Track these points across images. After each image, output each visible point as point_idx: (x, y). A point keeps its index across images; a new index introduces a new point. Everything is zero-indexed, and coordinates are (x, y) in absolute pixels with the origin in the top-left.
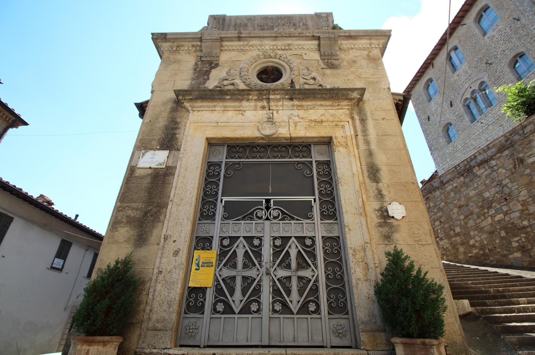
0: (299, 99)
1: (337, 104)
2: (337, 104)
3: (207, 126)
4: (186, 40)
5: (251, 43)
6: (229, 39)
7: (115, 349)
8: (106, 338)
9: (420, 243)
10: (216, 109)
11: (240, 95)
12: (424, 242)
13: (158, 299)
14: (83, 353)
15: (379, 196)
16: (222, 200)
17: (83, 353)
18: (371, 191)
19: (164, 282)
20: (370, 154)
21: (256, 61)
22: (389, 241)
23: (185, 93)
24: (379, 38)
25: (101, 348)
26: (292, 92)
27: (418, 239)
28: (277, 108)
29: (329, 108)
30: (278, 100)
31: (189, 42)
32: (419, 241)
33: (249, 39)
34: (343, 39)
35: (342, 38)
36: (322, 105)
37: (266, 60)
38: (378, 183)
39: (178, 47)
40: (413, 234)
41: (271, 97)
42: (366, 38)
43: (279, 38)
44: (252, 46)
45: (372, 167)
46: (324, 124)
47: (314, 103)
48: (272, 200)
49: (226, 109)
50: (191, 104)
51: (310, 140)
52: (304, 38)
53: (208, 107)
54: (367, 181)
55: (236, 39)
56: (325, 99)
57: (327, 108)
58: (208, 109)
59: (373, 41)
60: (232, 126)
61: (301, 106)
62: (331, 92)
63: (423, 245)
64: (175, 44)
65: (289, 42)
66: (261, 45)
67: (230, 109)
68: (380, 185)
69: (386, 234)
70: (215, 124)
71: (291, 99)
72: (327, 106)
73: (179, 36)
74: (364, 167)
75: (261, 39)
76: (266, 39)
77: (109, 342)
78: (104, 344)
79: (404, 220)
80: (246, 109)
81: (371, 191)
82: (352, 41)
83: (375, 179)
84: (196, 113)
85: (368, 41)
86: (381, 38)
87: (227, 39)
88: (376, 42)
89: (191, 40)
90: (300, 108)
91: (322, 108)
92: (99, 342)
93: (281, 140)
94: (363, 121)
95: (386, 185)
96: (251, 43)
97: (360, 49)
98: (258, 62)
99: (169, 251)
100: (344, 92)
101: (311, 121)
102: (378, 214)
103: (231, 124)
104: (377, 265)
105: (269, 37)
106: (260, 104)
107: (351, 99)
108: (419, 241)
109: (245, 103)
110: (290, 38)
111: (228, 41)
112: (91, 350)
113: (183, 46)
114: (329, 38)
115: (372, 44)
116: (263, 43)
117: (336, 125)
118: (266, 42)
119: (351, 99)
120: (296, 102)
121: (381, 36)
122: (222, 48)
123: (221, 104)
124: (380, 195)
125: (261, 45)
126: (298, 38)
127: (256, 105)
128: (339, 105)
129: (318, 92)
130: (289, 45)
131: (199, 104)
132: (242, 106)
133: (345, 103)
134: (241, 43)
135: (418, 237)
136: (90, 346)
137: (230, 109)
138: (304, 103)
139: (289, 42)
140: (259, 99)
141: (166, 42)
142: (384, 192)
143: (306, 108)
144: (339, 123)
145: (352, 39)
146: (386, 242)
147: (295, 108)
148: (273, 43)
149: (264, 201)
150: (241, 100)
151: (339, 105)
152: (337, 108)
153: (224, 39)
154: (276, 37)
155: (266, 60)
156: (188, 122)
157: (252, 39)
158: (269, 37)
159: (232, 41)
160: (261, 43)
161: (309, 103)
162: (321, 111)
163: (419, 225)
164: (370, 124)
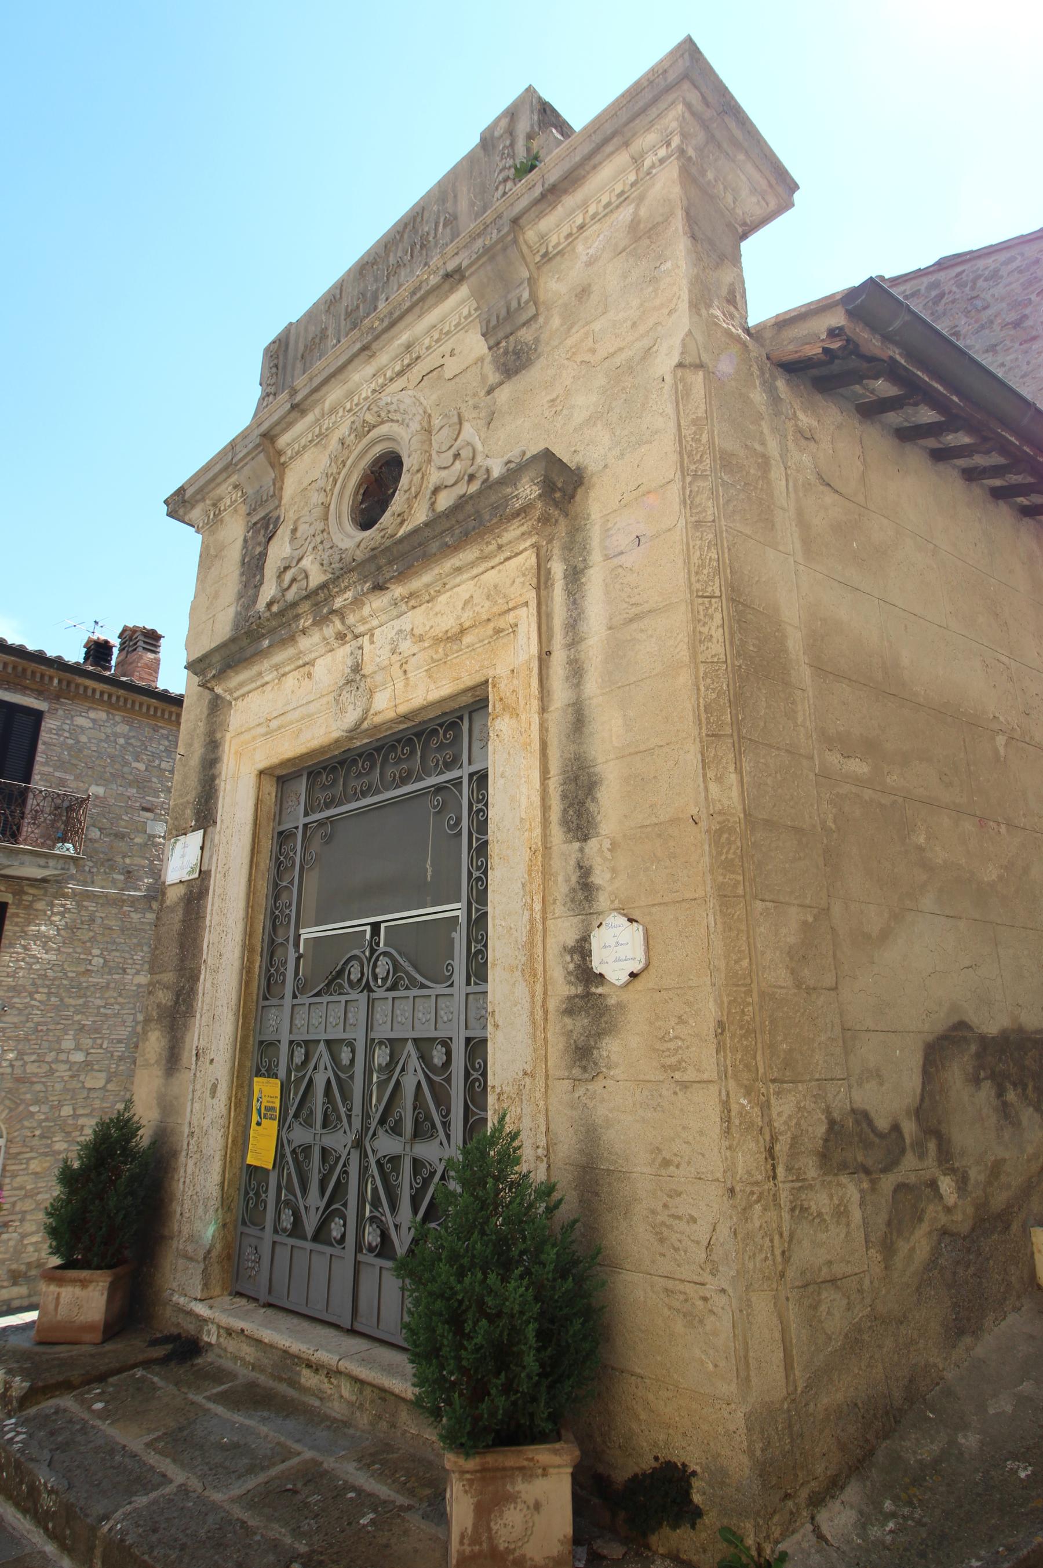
0: (401, 577)
1: (493, 547)
2: (493, 547)
3: (254, 738)
4: (218, 480)
5: (327, 405)
6: (283, 425)
7: (102, 1294)
8: (85, 1274)
9: (677, 1076)
10: (267, 679)
11: (282, 625)
12: (691, 1075)
13: (190, 1193)
14: (50, 1298)
15: (580, 895)
16: (298, 937)
17: (50, 1298)
18: (560, 879)
19: (198, 1156)
20: (579, 721)
21: (344, 463)
22: (585, 1069)
23: (202, 665)
24: (653, 112)
25: (77, 1291)
26: (373, 568)
27: (673, 1060)
28: (367, 626)
29: (481, 569)
30: (357, 602)
31: (225, 480)
32: (675, 1068)
33: (316, 396)
34: (540, 216)
35: (532, 214)
36: (458, 570)
37: (365, 441)
38: (585, 839)
39: (214, 505)
40: (662, 1039)
41: (338, 603)
42: (609, 148)
43: (374, 346)
44: (333, 410)
45: (576, 778)
46: (467, 639)
47: (437, 570)
48: (383, 925)
49: (281, 671)
50: (224, 685)
51: (454, 705)
52: (431, 300)
53: (252, 680)
54: (557, 833)
55: (294, 415)
56: (455, 548)
57: (475, 571)
58: (253, 685)
59: (636, 146)
60: (291, 723)
61: (411, 594)
62: (461, 517)
63: (685, 1085)
64: (208, 502)
65: (404, 338)
66: (349, 395)
67: (287, 669)
68: (593, 844)
69: (580, 1044)
70: (263, 730)
71: (379, 588)
72: (473, 564)
73: (202, 481)
74: (554, 784)
75: (340, 377)
76: (350, 367)
77: (91, 1282)
78: (84, 1284)
79: (639, 984)
80: (313, 656)
81: (560, 879)
82: (569, 201)
83: (579, 827)
84: (240, 703)
85: (622, 158)
86: (662, 105)
87: (278, 428)
88: (651, 138)
89: (225, 475)
90: (412, 603)
91: (465, 576)
92: (73, 1281)
93: (391, 728)
94: (575, 576)
95: (607, 844)
96: (327, 405)
97: (610, 209)
98: (349, 463)
99: (203, 1086)
100: (493, 498)
101: (437, 641)
102: (571, 966)
103: (290, 717)
104: (540, 1152)
105: (350, 361)
106: (329, 631)
107: (524, 511)
108: (675, 1068)
109: (304, 643)
110: (401, 325)
111: (285, 430)
112: (63, 1295)
113: (221, 499)
114: (487, 250)
115: (642, 155)
116: (350, 385)
117: (498, 631)
118: (356, 377)
119: (524, 511)
120: (398, 591)
121: (655, 100)
122: (282, 460)
123: (266, 664)
124: (585, 888)
125: (349, 395)
126: (417, 310)
127: (325, 639)
128: (500, 547)
129: (427, 533)
130: (408, 347)
131: (235, 679)
132: (301, 652)
133: (513, 532)
134: (310, 418)
135: (677, 1050)
136: (61, 1286)
137: (287, 669)
138: (416, 584)
139: (404, 338)
140: (321, 621)
141: (193, 507)
142: (600, 877)
143: (427, 598)
144: (501, 623)
145: (565, 191)
146: (576, 1072)
147: (404, 608)
148: (369, 370)
149: (368, 928)
150: (292, 639)
151: (500, 547)
152: (501, 557)
153: (273, 433)
154: (365, 348)
155: (365, 441)
156: (228, 736)
157: (325, 389)
158: (350, 361)
159: (290, 425)
160: (345, 387)
161: (426, 578)
162: (465, 588)
163: (687, 1003)
164: (595, 579)
